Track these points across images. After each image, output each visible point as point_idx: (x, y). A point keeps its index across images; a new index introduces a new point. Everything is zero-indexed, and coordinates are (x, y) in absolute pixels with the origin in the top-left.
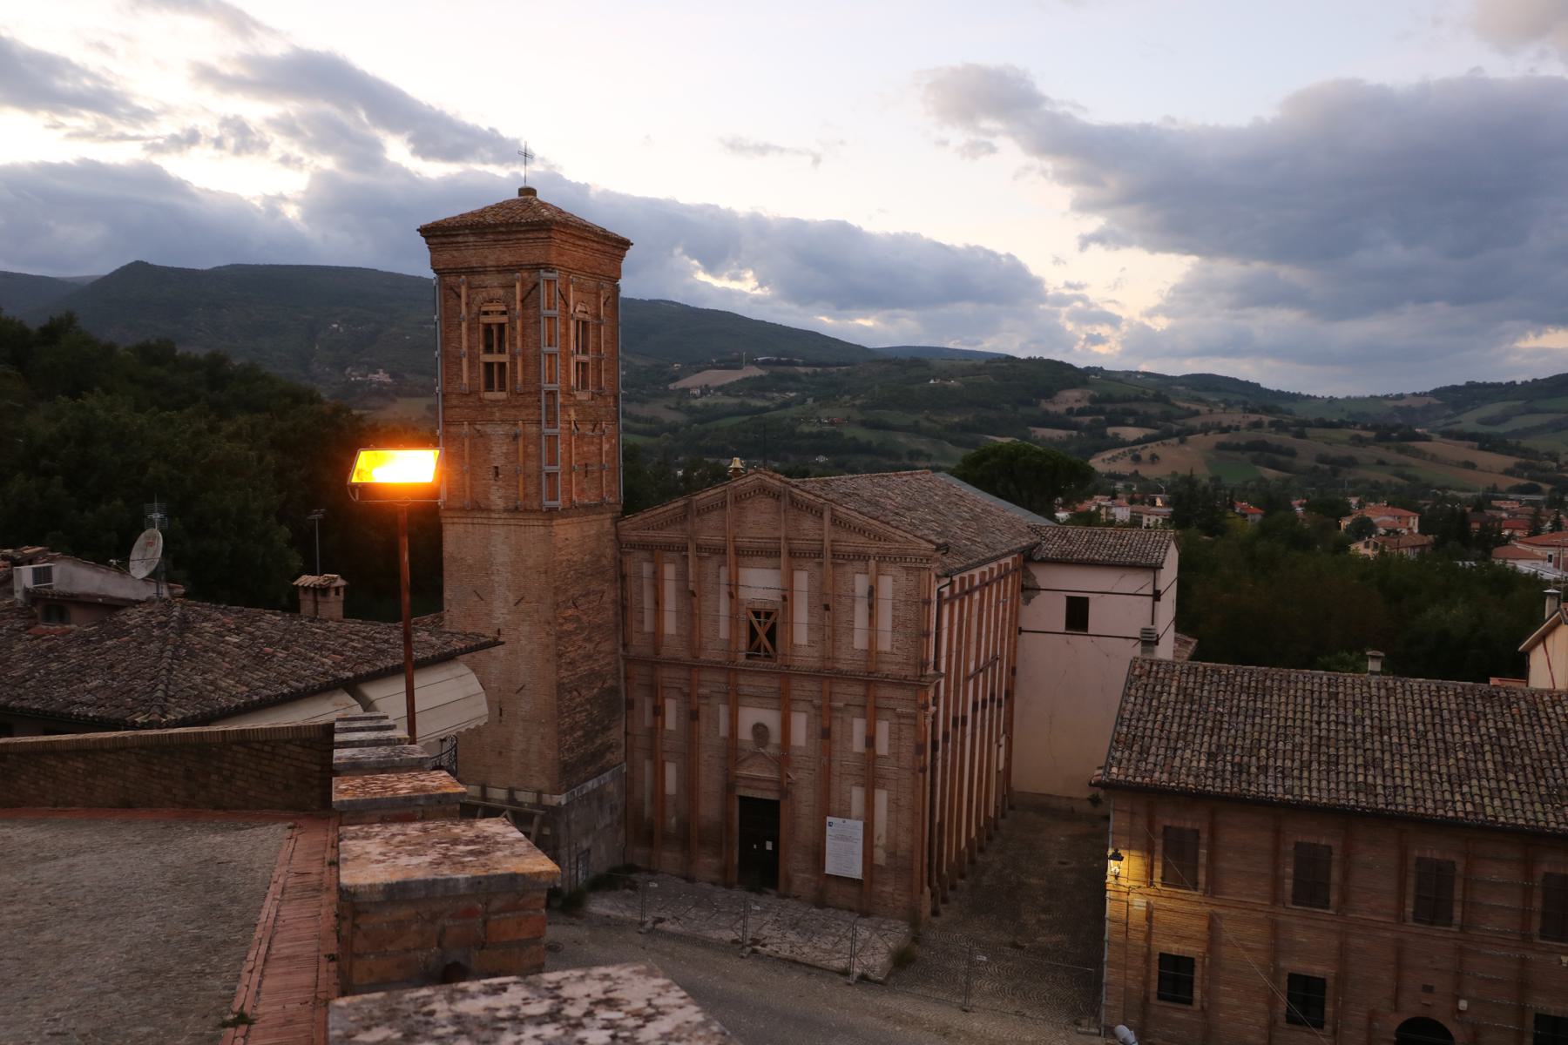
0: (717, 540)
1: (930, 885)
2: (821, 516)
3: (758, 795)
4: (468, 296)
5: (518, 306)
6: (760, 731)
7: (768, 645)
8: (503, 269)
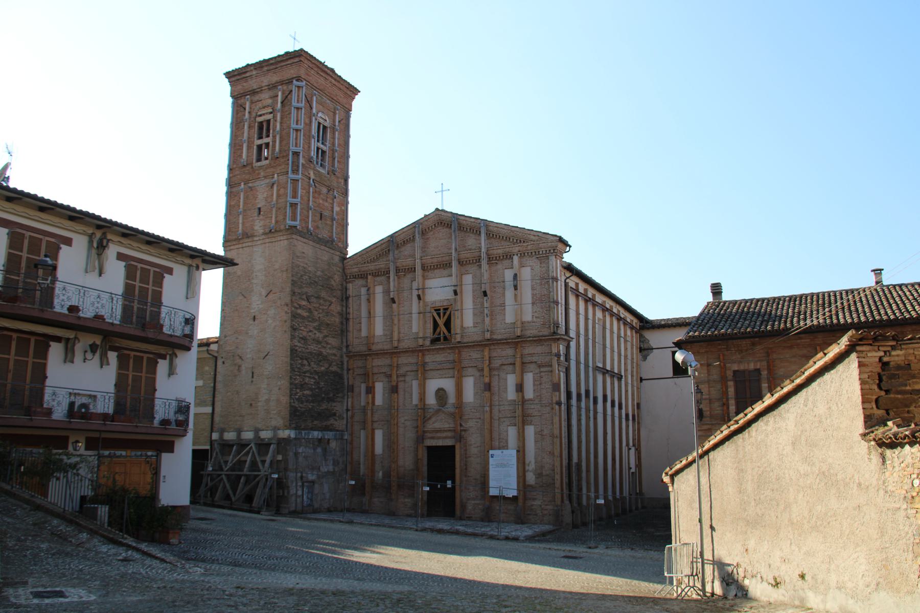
2: (480, 234)
3: (440, 443)
5: (279, 105)
7: (446, 331)
8: (272, 87)
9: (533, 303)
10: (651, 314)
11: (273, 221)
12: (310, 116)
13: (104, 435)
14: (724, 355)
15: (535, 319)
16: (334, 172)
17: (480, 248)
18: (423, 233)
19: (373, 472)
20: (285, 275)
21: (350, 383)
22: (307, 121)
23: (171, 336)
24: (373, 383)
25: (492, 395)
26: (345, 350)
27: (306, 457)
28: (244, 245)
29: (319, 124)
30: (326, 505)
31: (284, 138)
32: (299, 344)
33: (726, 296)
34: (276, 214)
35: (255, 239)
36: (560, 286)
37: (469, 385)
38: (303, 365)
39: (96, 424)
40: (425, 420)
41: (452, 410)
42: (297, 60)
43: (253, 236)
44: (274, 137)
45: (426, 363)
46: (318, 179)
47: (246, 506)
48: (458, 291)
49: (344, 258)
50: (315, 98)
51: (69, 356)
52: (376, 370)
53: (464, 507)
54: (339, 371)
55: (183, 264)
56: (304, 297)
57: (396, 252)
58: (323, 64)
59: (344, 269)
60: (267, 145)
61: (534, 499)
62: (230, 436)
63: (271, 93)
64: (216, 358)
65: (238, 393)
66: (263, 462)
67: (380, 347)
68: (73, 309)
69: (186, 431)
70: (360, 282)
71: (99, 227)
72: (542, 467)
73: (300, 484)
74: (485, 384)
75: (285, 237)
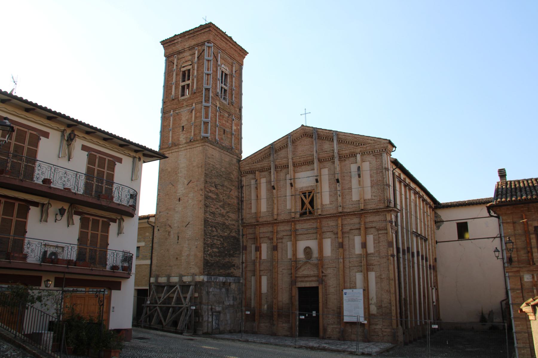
1: (401, 325)
3: (308, 285)
5: (196, 59)
6: (308, 251)
8: (192, 48)
9: (372, 187)
10: (442, 199)
11: (192, 134)
12: (216, 66)
13: (67, 276)
14: (526, 215)
16: (232, 104)
17: (333, 150)
18: (293, 142)
19: (261, 305)
21: (244, 244)
22: (215, 69)
23: (119, 204)
24: (260, 244)
25: (344, 251)
26: (240, 222)
27: (214, 295)
28: (173, 151)
29: (222, 72)
30: (228, 329)
31: (200, 80)
32: (210, 217)
33: (509, 178)
34: (194, 130)
35: (181, 146)
36: (390, 173)
37: (328, 244)
38: (213, 231)
39: (61, 267)
40: (297, 269)
41: (315, 262)
42: (207, 30)
43: (179, 145)
44: (193, 80)
45: (297, 230)
46: (222, 107)
47: (173, 329)
48: (319, 180)
49: (239, 160)
50: (219, 55)
51: (44, 218)
52: (262, 235)
53: (325, 330)
54: (237, 236)
55: (129, 156)
56: (213, 185)
57: (275, 155)
58: (225, 33)
59: (239, 168)
60: (188, 85)
61: (376, 324)
62: (162, 280)
63: (191, 52)
64: (154, 227)
65: (168, 250)
66: (185, 298)
67: (264, 219)
68: (46, 181)
69: (129, 274)
70: (251, 176)
71: (69, 126)
72: (382, 301)
73: (210, 313)
74: (339, 243)
75: (200, 145)
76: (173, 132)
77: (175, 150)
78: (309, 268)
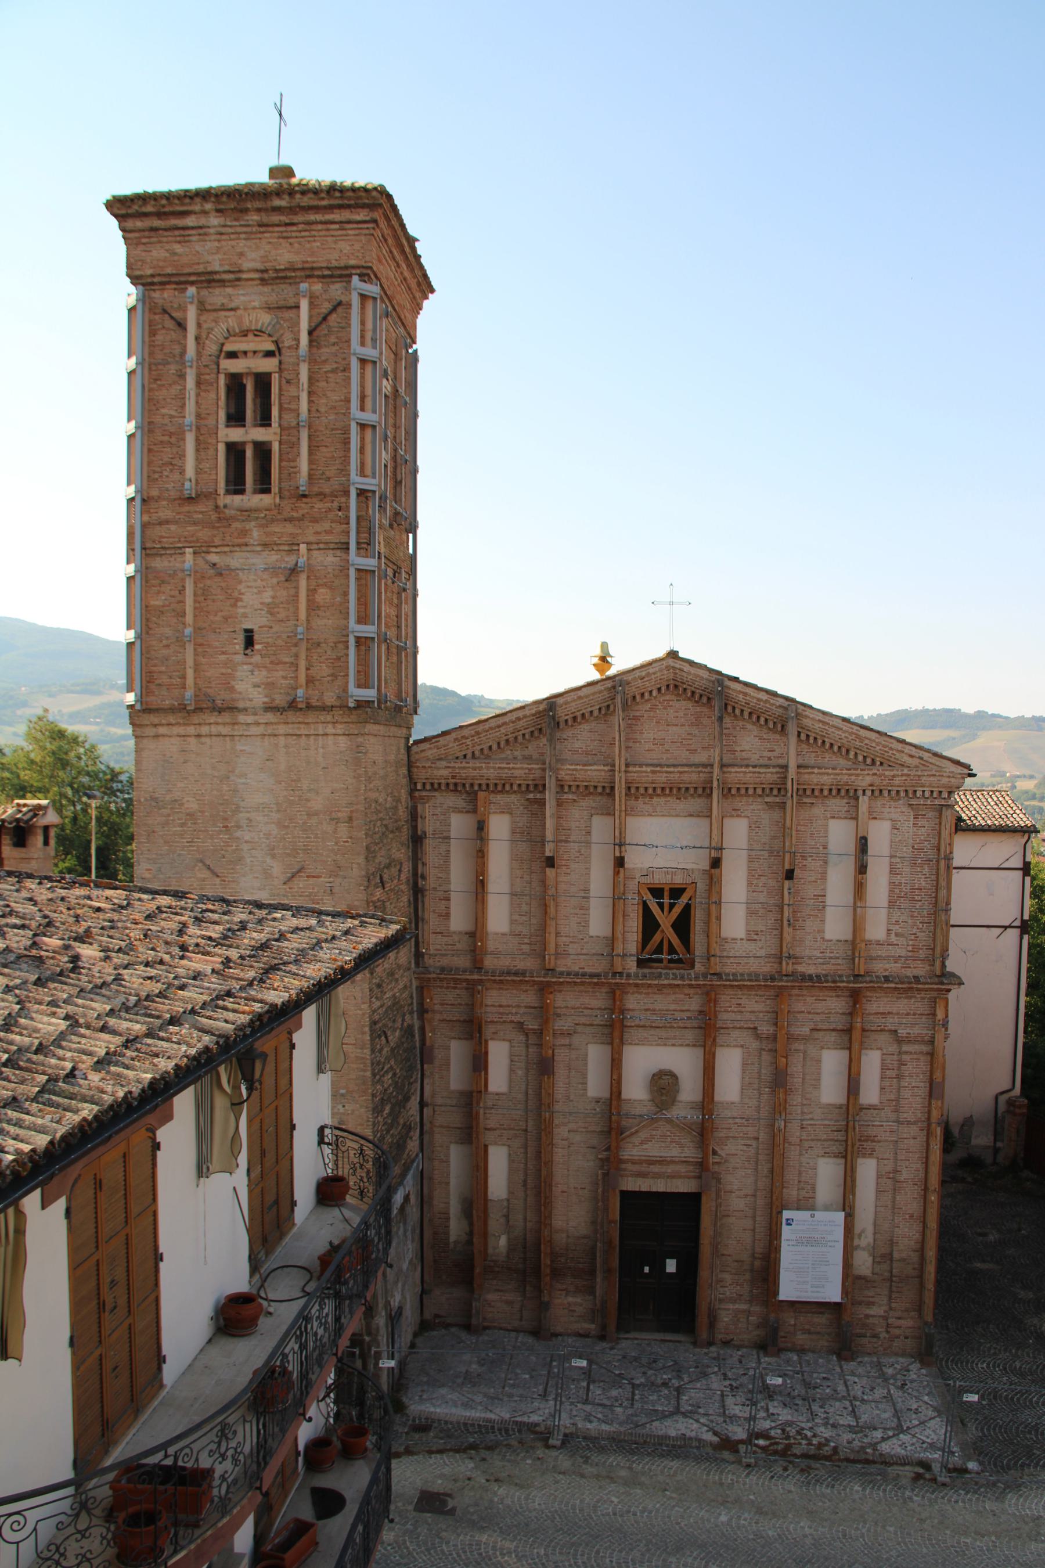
0: (596, 773)
4: (199, 325)
7: (676, 941)
8: (273, 277)
9: (892, 904)
15: (893, 938)
20: (343, 830)
28: (205, 730)
35: (242, 718)
37: (731, 1066)
42: (361, 215)
67: (505, 963)
72: (892, 1243)
75: (340, 729)
76: (197, 645)
77: (214, 729)
78: (664, 1136)
